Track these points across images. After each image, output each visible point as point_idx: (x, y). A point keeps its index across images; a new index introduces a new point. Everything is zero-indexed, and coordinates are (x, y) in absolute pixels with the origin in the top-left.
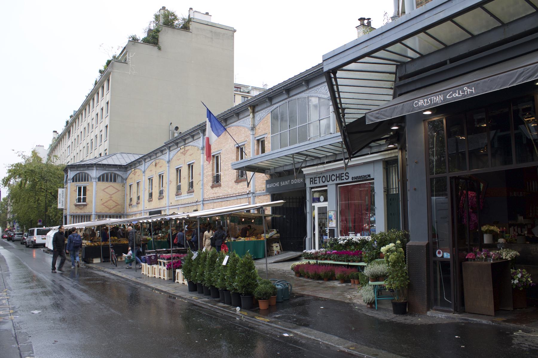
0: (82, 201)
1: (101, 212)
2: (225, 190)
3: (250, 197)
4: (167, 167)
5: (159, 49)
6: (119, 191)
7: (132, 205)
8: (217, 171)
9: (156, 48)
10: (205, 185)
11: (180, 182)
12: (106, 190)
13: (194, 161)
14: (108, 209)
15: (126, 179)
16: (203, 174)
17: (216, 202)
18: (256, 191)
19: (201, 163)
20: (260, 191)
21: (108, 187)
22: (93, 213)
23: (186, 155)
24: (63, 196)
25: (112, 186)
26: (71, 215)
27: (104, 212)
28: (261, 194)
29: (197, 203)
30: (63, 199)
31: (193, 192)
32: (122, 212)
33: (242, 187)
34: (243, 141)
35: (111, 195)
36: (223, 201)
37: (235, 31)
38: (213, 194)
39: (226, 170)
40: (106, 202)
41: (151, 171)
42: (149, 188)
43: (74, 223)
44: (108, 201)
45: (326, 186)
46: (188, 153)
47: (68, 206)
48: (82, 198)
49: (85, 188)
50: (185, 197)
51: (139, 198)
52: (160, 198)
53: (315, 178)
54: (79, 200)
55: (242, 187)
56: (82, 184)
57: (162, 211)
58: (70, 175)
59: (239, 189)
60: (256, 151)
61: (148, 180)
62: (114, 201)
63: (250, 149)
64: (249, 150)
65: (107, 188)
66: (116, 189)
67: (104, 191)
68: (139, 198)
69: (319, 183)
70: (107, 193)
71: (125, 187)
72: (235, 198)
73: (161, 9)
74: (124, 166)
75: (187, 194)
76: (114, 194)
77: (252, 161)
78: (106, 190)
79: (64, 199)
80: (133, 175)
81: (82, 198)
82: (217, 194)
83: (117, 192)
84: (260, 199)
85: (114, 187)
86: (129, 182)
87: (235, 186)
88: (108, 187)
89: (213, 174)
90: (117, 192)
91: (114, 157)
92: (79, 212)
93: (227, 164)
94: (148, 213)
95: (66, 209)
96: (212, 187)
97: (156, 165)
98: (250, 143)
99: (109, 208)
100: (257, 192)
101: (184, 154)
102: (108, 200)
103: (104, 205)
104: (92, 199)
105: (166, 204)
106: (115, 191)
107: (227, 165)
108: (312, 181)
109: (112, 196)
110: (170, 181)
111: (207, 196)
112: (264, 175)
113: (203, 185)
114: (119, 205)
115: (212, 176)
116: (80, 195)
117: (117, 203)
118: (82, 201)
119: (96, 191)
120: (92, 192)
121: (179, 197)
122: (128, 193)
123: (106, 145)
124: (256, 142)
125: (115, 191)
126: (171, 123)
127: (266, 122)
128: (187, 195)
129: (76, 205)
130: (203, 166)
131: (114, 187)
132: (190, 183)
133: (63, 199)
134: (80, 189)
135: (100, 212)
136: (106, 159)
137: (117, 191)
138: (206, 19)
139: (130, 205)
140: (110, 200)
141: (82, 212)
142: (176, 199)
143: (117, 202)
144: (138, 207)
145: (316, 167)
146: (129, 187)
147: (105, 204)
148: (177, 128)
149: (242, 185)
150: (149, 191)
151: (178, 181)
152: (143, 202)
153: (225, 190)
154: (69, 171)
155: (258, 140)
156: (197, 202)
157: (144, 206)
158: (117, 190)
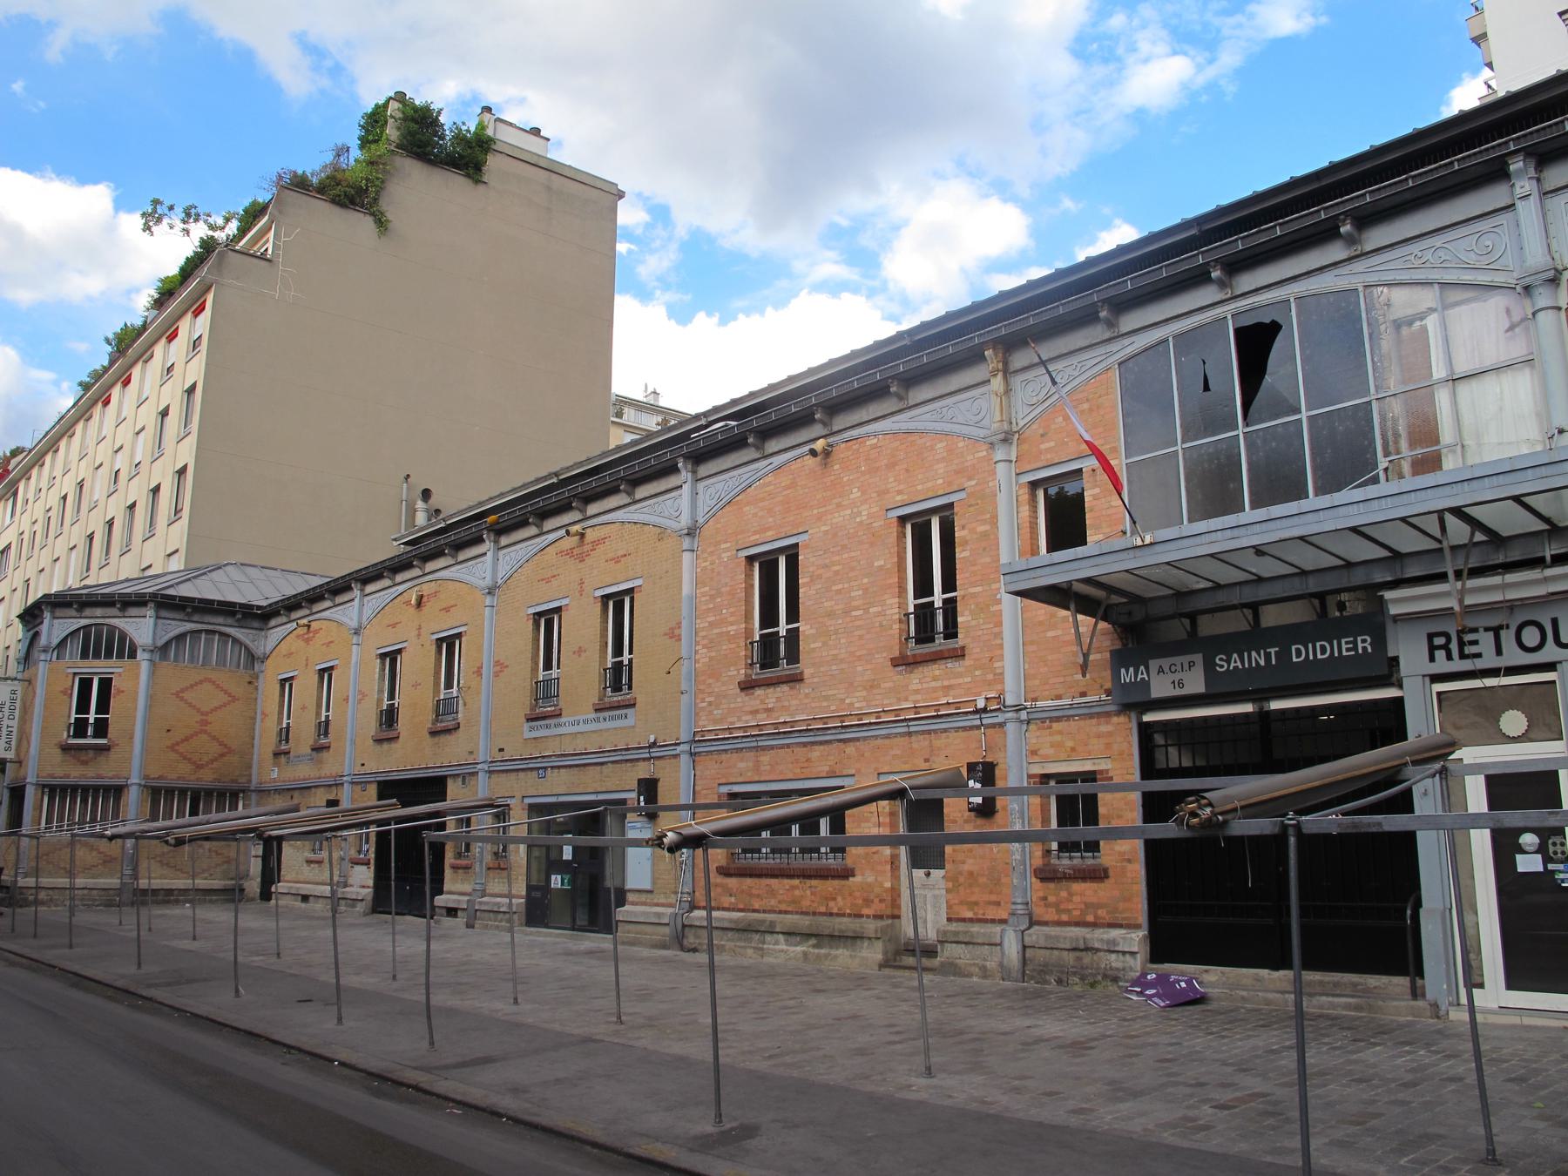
0: (90, 731)
1: (166, 778)
5: (381, 223)
6: (234, 699)
7: (288, 753)
9: (368, 222)
12: (185, 695)
17: (764, 748)
18: (1035, 700)
21: (196, 684)
22: (134, 780)
24: (12, 710)
25: (209, 680)
26: (44, 786)
27: (174, 776)
28: (1071, 712)
29: (656, 752)
30: (11, 723)
31: (633, 705)
32: (243, 780)
34: (940, 493)
35: (207, 714)
36: (813, 743)
37: (621, 195)
40: (186, 739)
43: (197, 814)
44: (192, 736)
45: (1550, 667)
47: (34, 750)
48: (91, 721)
49: (106, 684)
50: (582, 728)
52: (440, 725)
53: (1460, 633)
54: (80, 728)
55: (939, 684)
56: (97, 667)
57: (450, 782)
58: (49, 635)
59: (917, 692)
61: (378, 661)
62: (214, 738)
65: (192, 686)
66: (226, 692)
67: (182, 699)
69: (1499, 652)
70: (190, 705)
71: (256, 688)
73: (391, 98)
74: (259, 607)
75: (593, 715)
76: (216, 709)
77: (1158, 548)
78: (185, 695)
79: (15, 723)
80: (301, 643)
81: (91, 721)
82: (775, 714)
84: (1060, 733)
85: (218, 686)
88: (196, 684)
92: (76, 773)
93: (834, 588)
94: (373, 790)
95: (20, 762)
96: (747, 686)
99: (194, 763)
100: (1039, 704)
101: (579, 555)
103: (177, 752)
104: (134, 725)
107: (839, 592)
108: (1446, 647)
109: (210, 718)
114: (230, 751)
115: (747, 638)
116: (83, 706)
118: (90, 731)
119: (151, 698)
120: (135, 700)
121: (548, 727)
123: (177, 536)
124: (1024, 494)
126: (408, 476)
127: (1086, 406)
128: (597, 720)
129: (66, 748)
131: (218, 686)
132: (605, 670)
133: (11, 723)
134: (85, 685)
135: (160, 778)
136: (189, 580)
137: (226, 698)
138: (531, 144)
140: (202, 731)
141: (91, 774)
142: (528, 735)
144: (320, 762)
145: (1496, 580)
146: (278, 686)
147: (181, 748)
148: (426, 494)
149: (937, 673)
151: (537, 664)
154: (47, 615)
156: (654, 745)
158: (230, 695)
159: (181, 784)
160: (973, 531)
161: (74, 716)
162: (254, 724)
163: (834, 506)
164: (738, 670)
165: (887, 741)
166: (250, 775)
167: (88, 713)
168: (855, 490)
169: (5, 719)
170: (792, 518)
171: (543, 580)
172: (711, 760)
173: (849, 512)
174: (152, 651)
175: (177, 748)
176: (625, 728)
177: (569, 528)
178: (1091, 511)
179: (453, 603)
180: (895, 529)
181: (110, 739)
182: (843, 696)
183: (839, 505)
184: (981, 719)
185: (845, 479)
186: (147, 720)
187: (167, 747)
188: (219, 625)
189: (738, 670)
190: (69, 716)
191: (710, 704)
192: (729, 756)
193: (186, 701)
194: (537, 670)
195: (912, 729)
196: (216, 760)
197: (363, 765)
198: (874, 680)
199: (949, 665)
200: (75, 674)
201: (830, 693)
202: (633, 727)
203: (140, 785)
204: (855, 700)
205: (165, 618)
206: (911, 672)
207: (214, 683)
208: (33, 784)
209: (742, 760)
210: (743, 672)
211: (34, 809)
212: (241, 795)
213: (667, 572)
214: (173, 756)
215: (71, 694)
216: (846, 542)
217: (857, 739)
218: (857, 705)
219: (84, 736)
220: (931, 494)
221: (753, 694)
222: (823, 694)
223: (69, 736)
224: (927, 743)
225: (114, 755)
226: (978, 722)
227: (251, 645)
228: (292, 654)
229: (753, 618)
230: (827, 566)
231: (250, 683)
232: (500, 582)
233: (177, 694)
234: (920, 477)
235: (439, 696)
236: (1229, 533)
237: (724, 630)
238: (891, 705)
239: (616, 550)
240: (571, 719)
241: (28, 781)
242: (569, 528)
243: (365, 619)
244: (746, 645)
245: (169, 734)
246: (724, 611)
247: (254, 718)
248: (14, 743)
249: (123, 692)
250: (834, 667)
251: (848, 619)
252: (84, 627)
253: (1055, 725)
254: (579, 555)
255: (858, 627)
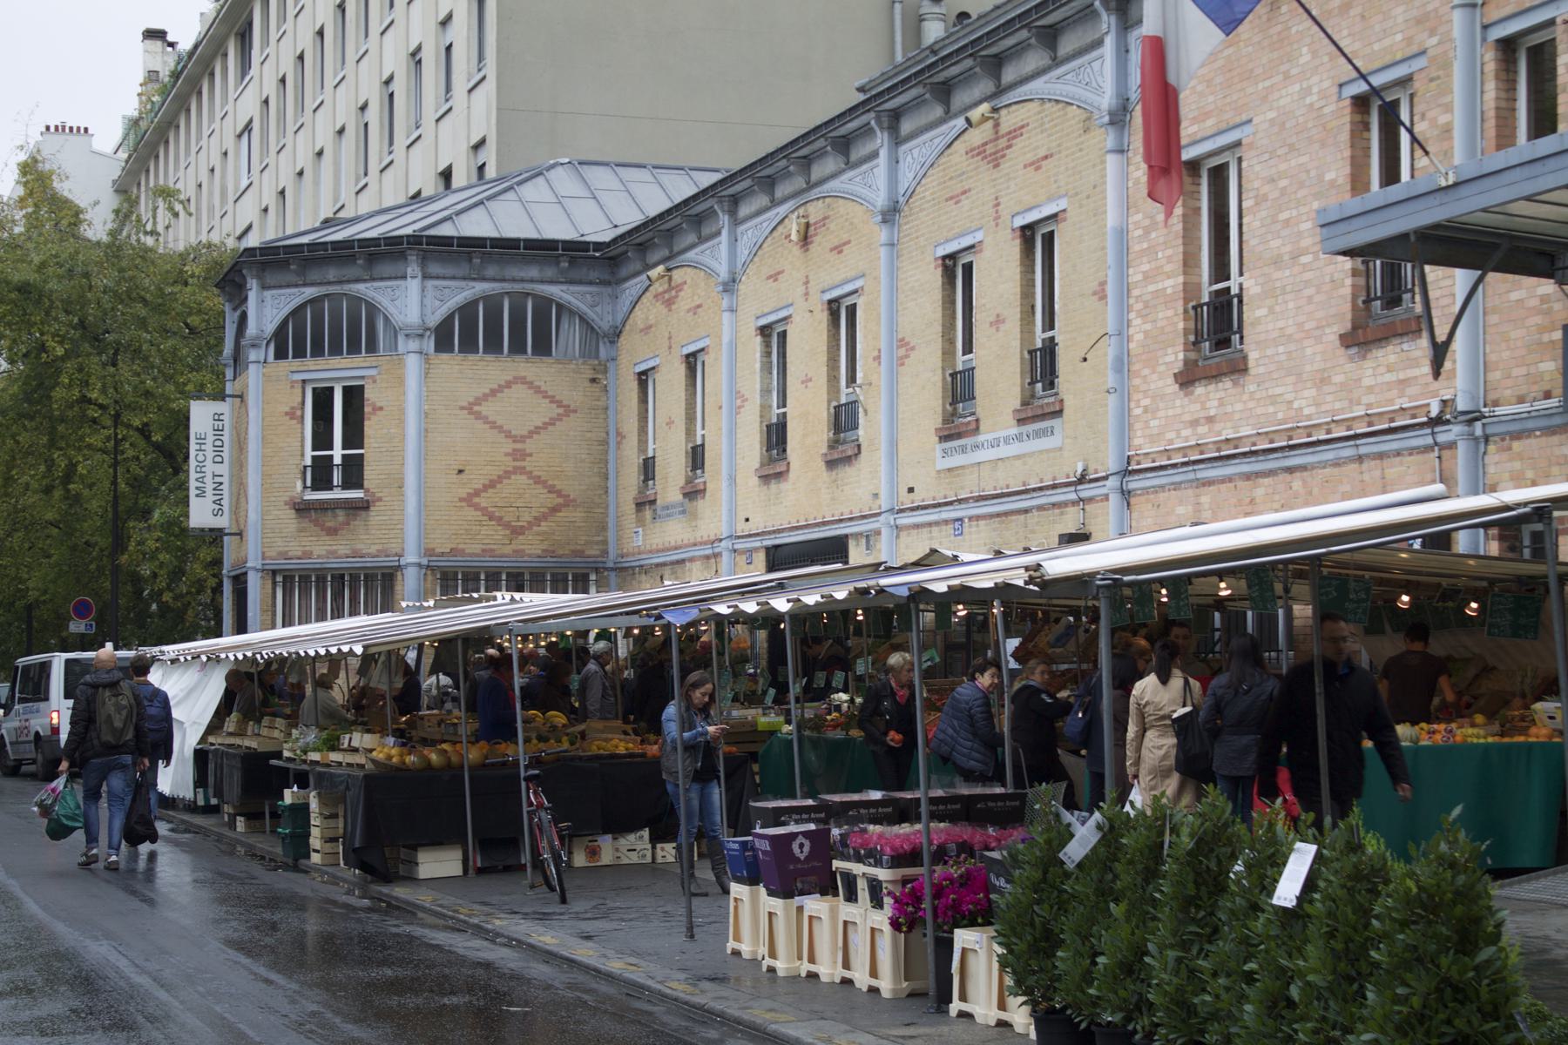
0: (337, 477)
2: (1273, 400)
3: (1452, 445)
4: (883, 252)
6: (568, 411)
8: (1220, 269)
10: (1135, 367)
11: (968, 348)
12: (485, 409)
13: (1063, 204)
14: (500, 534)
15: (615, 335)
16: (1125, 290)
17: (1209, 483)
18: (1496, 403)
19: (1111, 219)
20: (1521, 400)
21: (500, 389)
22: (411, 557)
23: (1005, 166)
24: (218, 450)
25: (522, 380)
26: (274, 572)
27: (477, 548)
28: (1530, 424)
29: (1086, 491)
30: (219, 469)
32: (593, 551)
33: (1389, 377)
34: (1399, 56)
36: (1259, 474)
38: (1194, 423)
39: (1277, 262)
40: (492, 485)
41: (774, 277)
42: (766, 391)
44: (500, 479)
46: (1022, 151)
47: (253, 516)
48: (337, 460)
49: (354, 396)
51: (697, 457)
54: (321, 474)
55: (1389, 377)
56: (337, 370)
58: (259, 318)
59: (1370, 389)
60: (1491, 123)
61: (759, 339)
62: (538, 480)
63: (1448, 108)
64: (1443, 119)
65: (493, 392)
66: (553, 400)
67: (478, 416)
68: (697, 457)
70: (493, 425)
71: (605, 389)
72: (1347, 451)
74: (598, 246)
75: (1014, 431)
76: (537, 430)
78: (485, 409)
79: (224, 469)
80: (660, 308)
81: (337, 460)
82: (1218, 427)
83: (559, 418)
84: (1520, 457)
85: (538, 390)
86: (633, 353)
87: (1345, 366)
88: (500, 389)
89: (1189, 290)
90: (559, 418)
91: (533, 191)
92: (322, 550)
93: (1283, 216)
94: (760, 559)
95: (240, 534)
96: (1187, 378)
97: (805, 239)
98: (1447, 66)
99: (507, 525)
100: (1500, 410)
102: (495, 472)
103: (477, 507)
105: (876, 495)
106: (545, 411)
107: (1287, 221)
109: (529, 446)
110: (902, 343)
111: (1152, 439)
112: (1547, 287)
113: (1122, 365)
114: (568, 502)
116: (322, 439)
117: (559, 493)
118: (337, 477)
120: (402, 422)
121: (963, 450)
122: (631, 425)
124: (1490, 60)
125: (545, 411)
128: (1019, 438)
129: (303, 509)
130: (1122, 234)
131: (538, 390)
133: (219, 469)
136: (481, 203)
139: (640, 506)
141: (343, 550)
143: (559, 484)
144: (694, 516)
147: (482, 501)
149: (1392, 358)
150: (765, 408)
152: (724, 484)
153: (1273, 400)
154: (253, 285)
155: (1508, 47)
156: (1082, 479)
157: (733, 512)
158: (559, 404)
159: (488, 561)
160: (1434, 121)
161: (309, 453)
162: (607, 452)
163: (1281, 77)
164: (1176, 353)
165: (1336, 471)
166: (605, 542)
167: (332, 449)
168: (1305, 50)
169: (209, 462)
170: (1235, 97)
171: (951, 198)
172: (1148, 501)
173: (1297, 87)
174: (421, 336)
175: (476, 500)
176: (1048, 451)
177: (969, 114)
178: (1564, 91)
179: (845, 237)
180: (1347, 119)
181: (367, 491)
182: (1289, 397)
183: (1287, 76)
184: (1433, 433)
185: (1294, 30)
186: (424, 455)
187: (461, 500)
188: (532, 281)
189: (1176, 353)
190: (303, 455)
191: (1146, 410)
192: (1166, 494)
193: (485, 420)
194: (953, 353)
195: (1363, 450)
196: (544, 517)
197: (747, 520)
198: (1324, 370)
199: (1405, 346)
200: (304, 381)
201: (1278, 391)
202: (1061, 449)
203: (420, 565)
204: (1304, 403)
205: (438, 278)
206: (1364, 358)
207: (530, 385)
208: (257, 570)
209: (1181, 503)
210: (1181, 356)
211: (263, 611)
212: (593, 577)
213: (1095, 187)
214: (471, 513)
215: (302, 417)
216: (1294, 139)
217: (1303, 468)
218: (1306, 411)
219: (328, 486)
220: (1388, 60)
221: (1192, 393)
222: (1270, 392)
223: (305, 487)
224: (1378, 473)
225: (376, 515)
226: (1430, 440)
227: (590, 314)
228: (651, 327)
229: (1198, 265)
230: (1273, 180)
231: (593, 380)
232: (901, 200)
233: (469, 408)
234: (1377, 28)
235: (838, 399)
236: (1527, 171)
237: (1160, 286)
238: (1342, 410)
239: (1037, 148)
240: (990, 437)
241: (248, 565)
242: (969, 114)
243: (739, 265)
244: (1186, 311)
245: (462, 476)
246: (1160, 255)
247: (605, 442)
248: (225, 502)
249: (381, 408)
250: (1281, 349)
251: (1296, 269)
252: (311, 301)
253: (1516, 445)
254: (992, 156)
255: (1307, 283)
